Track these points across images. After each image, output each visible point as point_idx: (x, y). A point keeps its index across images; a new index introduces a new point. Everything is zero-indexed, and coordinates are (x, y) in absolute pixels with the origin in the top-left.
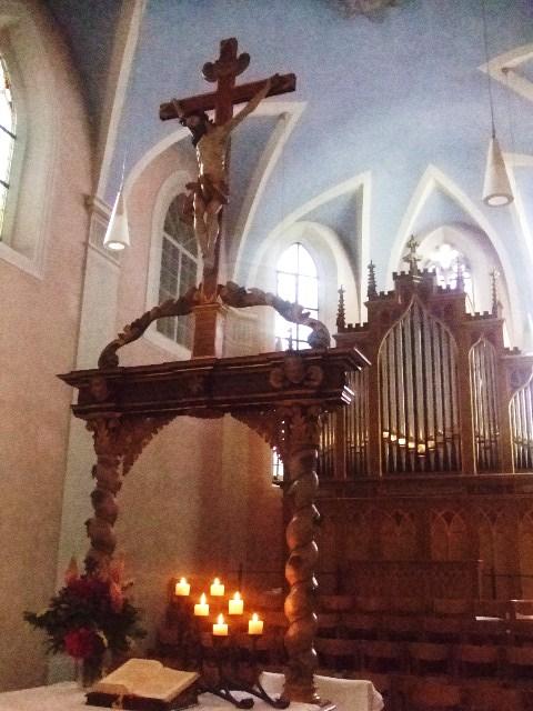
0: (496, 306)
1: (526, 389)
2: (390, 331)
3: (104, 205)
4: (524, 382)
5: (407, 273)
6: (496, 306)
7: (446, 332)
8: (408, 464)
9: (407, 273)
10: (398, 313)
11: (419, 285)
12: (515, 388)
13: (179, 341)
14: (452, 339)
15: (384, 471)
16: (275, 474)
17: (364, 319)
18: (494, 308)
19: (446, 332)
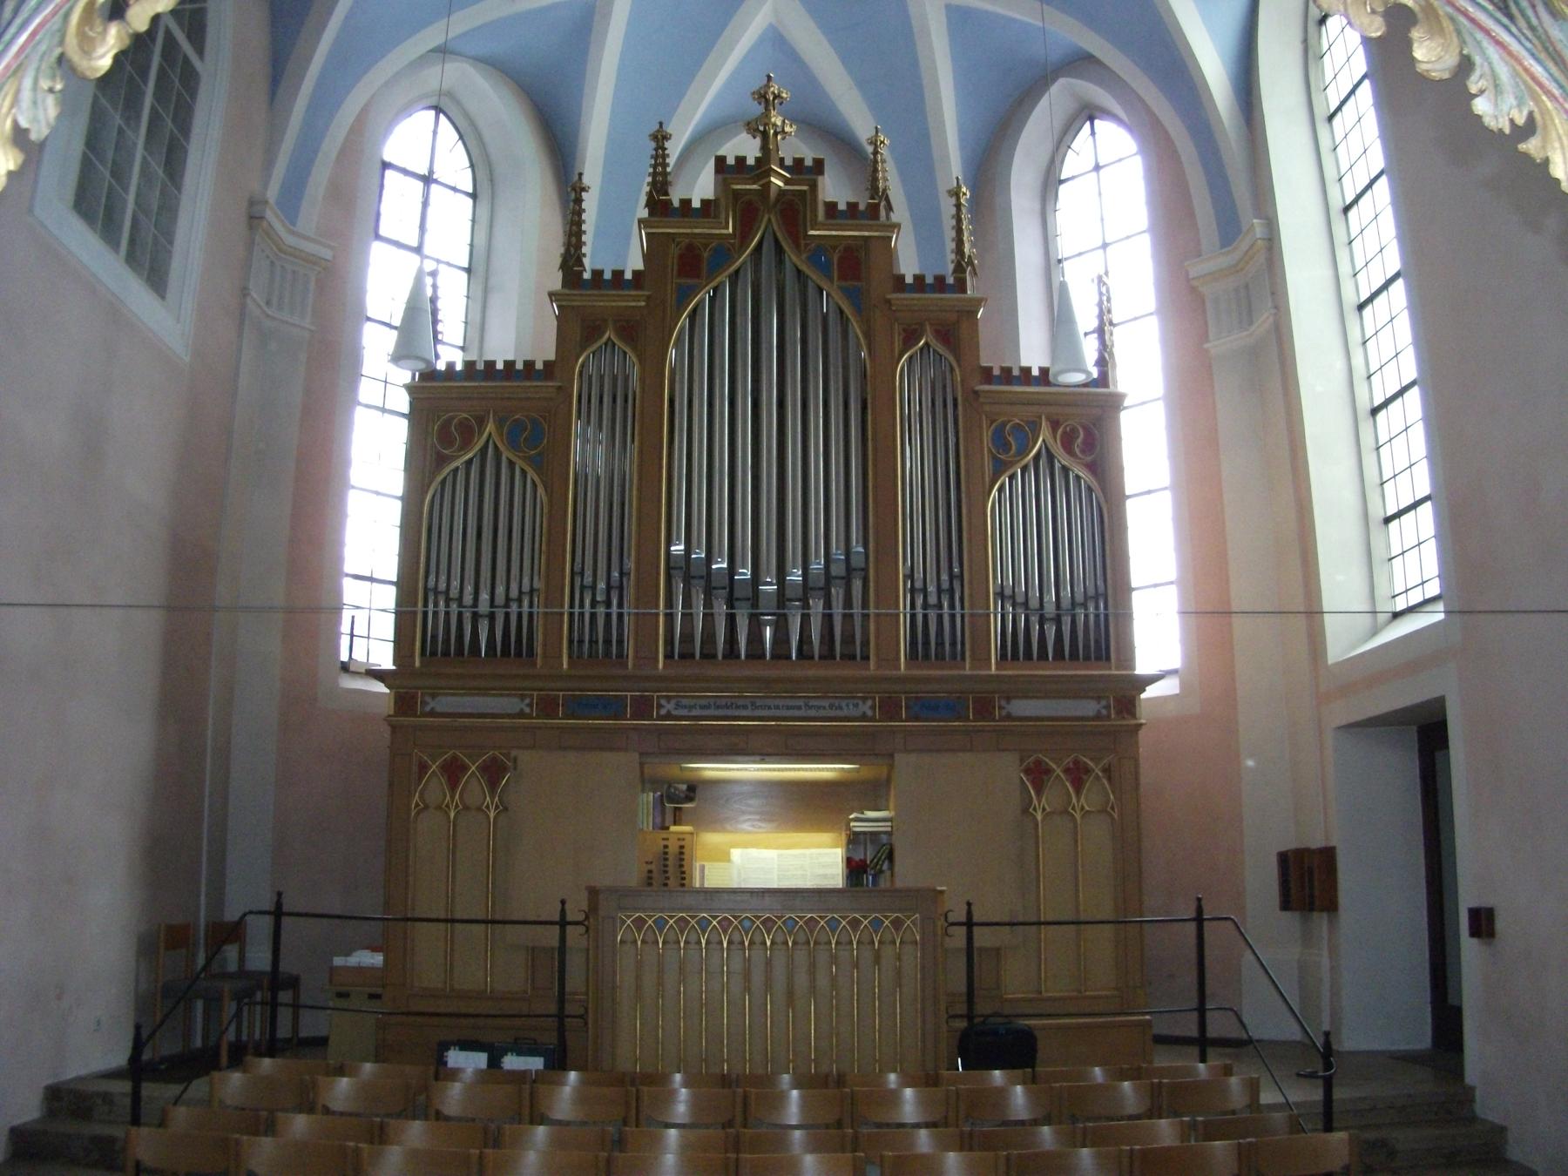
0: (962, 265)
1: (1024, 469)
2: (705, 295)
3: (319, 243)
4: (1023, 451)
5: (751, 161)
6: (962, 265)
7: (533, 482)
8: (709, 636)
9: (751, 161)
10: (724, 252)
11: (781, 192)
12: (1000, 467)
13: (132, 259)
14: (856, 328)
15: (669, 656)
16: (344, 657)
17: (634, 262)
18: (959, 269)
19: (533, 482)
